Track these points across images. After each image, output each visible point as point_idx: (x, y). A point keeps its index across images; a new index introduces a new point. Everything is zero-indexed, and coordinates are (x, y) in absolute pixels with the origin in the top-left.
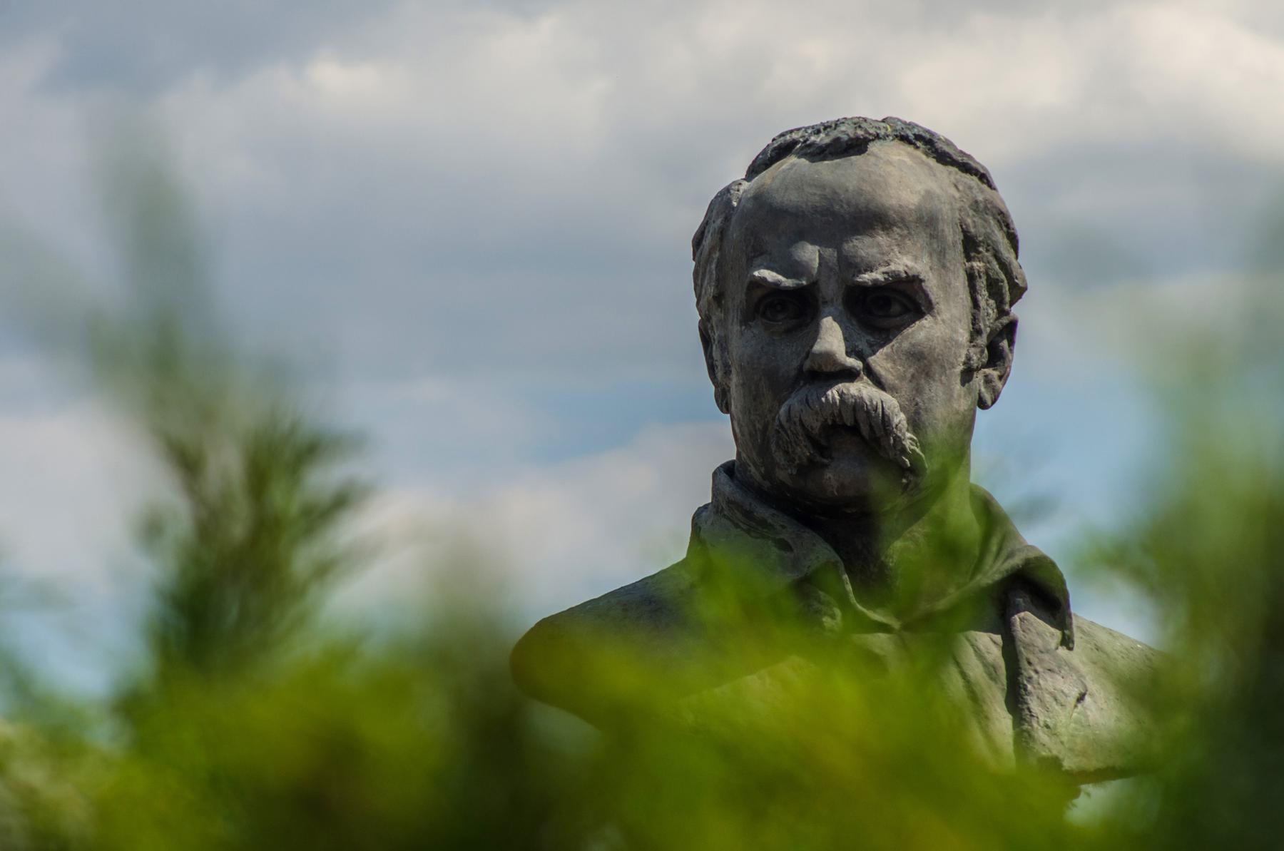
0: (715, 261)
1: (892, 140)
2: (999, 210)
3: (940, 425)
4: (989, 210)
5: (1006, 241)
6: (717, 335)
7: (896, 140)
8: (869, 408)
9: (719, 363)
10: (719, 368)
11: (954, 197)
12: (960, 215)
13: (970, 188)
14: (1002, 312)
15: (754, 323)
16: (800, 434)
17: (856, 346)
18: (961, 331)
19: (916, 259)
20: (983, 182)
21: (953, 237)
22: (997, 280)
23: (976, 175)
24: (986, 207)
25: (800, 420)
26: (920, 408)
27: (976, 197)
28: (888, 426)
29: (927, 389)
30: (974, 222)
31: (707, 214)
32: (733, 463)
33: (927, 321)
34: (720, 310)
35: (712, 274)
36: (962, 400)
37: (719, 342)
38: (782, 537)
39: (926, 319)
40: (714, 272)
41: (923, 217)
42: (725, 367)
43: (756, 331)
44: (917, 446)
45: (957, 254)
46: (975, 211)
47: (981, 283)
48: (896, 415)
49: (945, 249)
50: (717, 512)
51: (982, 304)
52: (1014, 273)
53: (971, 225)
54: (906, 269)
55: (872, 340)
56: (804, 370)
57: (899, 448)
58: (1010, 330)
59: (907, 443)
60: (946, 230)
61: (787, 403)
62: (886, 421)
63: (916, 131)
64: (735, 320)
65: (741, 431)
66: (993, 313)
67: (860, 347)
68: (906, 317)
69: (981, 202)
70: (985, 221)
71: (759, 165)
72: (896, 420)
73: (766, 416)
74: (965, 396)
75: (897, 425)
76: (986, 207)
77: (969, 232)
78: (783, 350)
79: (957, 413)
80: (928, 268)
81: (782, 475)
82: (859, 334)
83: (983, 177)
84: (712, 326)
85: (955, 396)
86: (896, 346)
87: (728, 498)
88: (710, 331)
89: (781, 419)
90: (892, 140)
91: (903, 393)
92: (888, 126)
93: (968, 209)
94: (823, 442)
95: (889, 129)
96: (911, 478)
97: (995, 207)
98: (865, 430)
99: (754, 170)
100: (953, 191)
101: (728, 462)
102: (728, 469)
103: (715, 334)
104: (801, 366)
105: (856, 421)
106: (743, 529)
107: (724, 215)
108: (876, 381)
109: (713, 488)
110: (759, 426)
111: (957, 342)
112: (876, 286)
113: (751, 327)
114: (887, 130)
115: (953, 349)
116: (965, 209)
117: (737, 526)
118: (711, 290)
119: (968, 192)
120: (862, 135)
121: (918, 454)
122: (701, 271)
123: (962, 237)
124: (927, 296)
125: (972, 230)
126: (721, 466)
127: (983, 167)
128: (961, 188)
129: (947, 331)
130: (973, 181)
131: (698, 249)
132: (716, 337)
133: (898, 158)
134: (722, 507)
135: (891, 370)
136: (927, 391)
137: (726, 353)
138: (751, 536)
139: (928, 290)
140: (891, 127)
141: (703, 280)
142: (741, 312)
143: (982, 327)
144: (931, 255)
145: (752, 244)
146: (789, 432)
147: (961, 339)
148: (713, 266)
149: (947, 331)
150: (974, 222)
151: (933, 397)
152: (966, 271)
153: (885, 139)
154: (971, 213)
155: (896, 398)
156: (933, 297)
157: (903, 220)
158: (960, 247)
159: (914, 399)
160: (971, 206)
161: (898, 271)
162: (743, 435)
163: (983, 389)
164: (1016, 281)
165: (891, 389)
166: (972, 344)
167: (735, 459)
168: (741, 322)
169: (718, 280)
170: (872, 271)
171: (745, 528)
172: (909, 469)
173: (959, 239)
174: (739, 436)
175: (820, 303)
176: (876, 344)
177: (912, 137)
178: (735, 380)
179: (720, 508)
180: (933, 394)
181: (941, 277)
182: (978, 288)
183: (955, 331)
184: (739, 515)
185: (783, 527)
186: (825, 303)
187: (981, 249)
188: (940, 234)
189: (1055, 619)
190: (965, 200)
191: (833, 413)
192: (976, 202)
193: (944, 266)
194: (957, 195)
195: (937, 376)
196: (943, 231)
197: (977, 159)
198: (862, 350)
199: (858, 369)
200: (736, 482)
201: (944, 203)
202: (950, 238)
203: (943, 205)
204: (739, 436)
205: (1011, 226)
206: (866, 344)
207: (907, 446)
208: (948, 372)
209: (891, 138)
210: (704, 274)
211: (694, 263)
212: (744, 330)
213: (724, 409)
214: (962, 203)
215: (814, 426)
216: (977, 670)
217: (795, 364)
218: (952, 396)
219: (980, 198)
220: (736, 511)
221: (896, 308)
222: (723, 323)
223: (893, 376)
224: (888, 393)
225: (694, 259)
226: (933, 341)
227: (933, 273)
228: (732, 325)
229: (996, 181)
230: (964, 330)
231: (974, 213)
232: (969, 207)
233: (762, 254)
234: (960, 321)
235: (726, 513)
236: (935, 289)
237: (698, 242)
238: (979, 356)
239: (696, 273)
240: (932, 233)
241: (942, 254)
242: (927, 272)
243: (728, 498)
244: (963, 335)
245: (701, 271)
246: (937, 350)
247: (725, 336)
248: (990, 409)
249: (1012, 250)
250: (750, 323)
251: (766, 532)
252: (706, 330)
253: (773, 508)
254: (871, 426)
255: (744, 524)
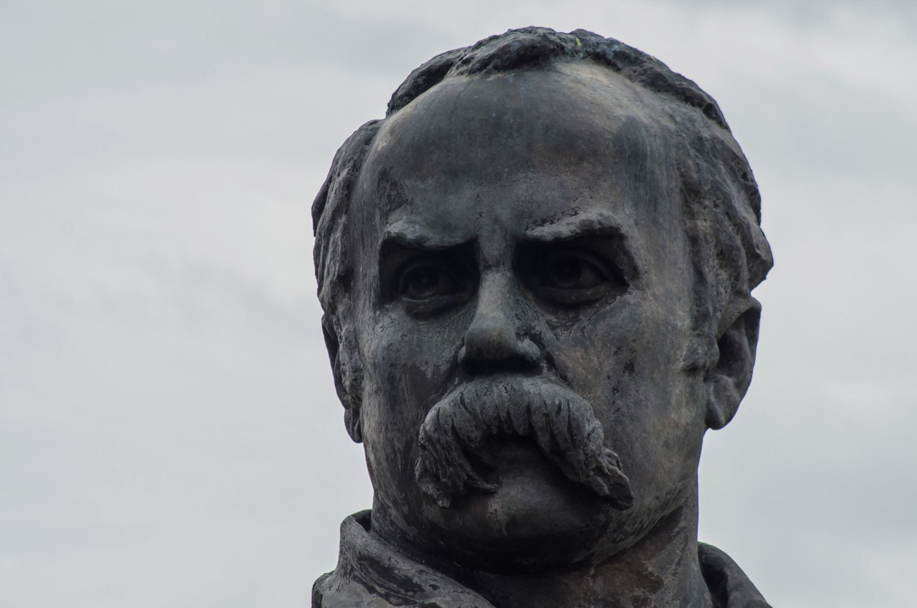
0: (341, 227)
1: (583, 58)
2: (734, 153)
3: (651, 441)
4: (718, 151)
5: (743, 195)
6: (344, 330)
7: (589, 58)
8: (550, 408)
9: (347, 368)
10: (347, 373)
11: (668, 129)
12: (677, 154)
13: (692, 120)
14: (741, 294)
15: (391, 306)
16: (453, 447)
17: (532, 328)
18: (680, 313)
19: (614, 208)
20: (710, 117)
21: (668, 182)
22: (731, 246)
23: (700, 106)
24: (713, 148)
25: (453, 428)
26: (623, 415)
27: (699, 132)
28: (576, 435)
29: (633, 389)
30: (697, 164)
31: (332, 167)
32: (369, 512)
33: (632, 297)
34: (347, 295)
35: (336, 246)
36: (684, 410)
37: (346, 339)
38: (432, 601)
39: (630, 293)
40: (339, 243)
41: (625, 151)
42: (355, 372)
43: (394, 316)
44: (618, 466)
45: (672, 205)
46: (698, 150)
47: (709, 252)
48: (588, 420)
49: (656, 199)
50: (345, 574)
51: (710, 278)
52: (755, 241)
53: (693, 168)
54: (600, 218)
55: (555, 320)
56: (459, 360)
57: (594, 466)
58: (752, 317)
59: (605, 462)
60: (657, 171)
61: (436, 406)
62: (574, 427)
63: (616, 47)
64: (368, 303)
65: (375, 458)
66: (725, 296)
67: (538, 328)
68: (603, 288)
69: (707, 140)
70: (714, 165)
71: (401, 97)
72: (588, 428)
73: (408, 430)
74: (687, 403)
75: (589, 435)
76: (713, 148)
77: (691, 178)
78: (432, 337)
79: (677, 426)
80: (631, 222)
81: (431, 513)
82: (536, 312)
83: (710, 109)
84: (338, 319)
85: (673, 402)
86: (588, 328)
87: (360, 553)
88: (335, 327)
89: (427, 428)
90: (583, 58)
91: (599, 393)
92: (578, 40)
93: (689, 147)
94: (486, 458)
95: (579, 44)
96: (614, 513)
97: (728, 149)
98: (543, 440)
99: (395, 104)
100: (666, 122)
101: (363, 511)
102: (363, 519)
103: (341, 330)
104: (456, 356)
105: (531, 427)
106: (381, 595)
107: (351, 163)
108: (561, 375)
109: (341, 542)
110: (399, 445)
111: (675, 327)
112: (558, 243)
113: (387, 310)
114: (576, 44)
115: (670, 336)
116: (684, 147)
117: (371, 590)
118: (334, 268)
119: (689, 125)
120: (539, 42)
121: (620, 477)
122: (323, 245)
123: (680, 184)
124: (631, 259)
125: (695, 176)
126: (353, 515)
127: (709, 96)
128: (678, 119)
129: (660, 310)
130: (697, 114)
131: (319, 219)
132: (342, 334)
133: (591, 76)
134: (352, 567)
135: (581, 360)
136: (633, 392)
137: (357, 353)
138: (391, 603)
139: (633, 251)
140: (581, 40)
141: (325, 256)
142: (375, 291)
143: (711, 309)
144: (636, 205)
145: (386, 194)
146: (438, 446)
147: (680, 324)
148: (338, 234)
149: (660, 310)
150: (697, 164)
151: (641, 400)
152: (687, 233)
153: (573, 56)
154: (693, 152)
155: (589, 399)
156: (640, 264)
157: (595, 153)
158: (677, 198)
159: (614, 402)
160: (693, 144)
161: (590, 220)
162: (379, 463)
163: (713, 399)
164: (758, 251)
165: (583, 388)
166: (696, 332)
167: (370, 506)
168: (374, 306)
169: (344, 253)
170: (552, 223)
171: (383, 592)
172: (609, 500)
173: (676, 186)
174: (374, 465)
175: (481, 268)
176: (561, 326)
177: (610, 56)
178: (368, 386)
179: (349, 568)
180: (641, 397)
181: (650, 236)
182: (703, 255)
183: (673, 312)
184: (375, 575)
185: (435, 587)
186: (488, 267)
187: (707, 203)
188: (648, 177)
189: (693, 247)
190: (684, 135)
191: (499, 417)
192: (700, 139)
193: (655, 222)
194: (672, 127)
195: (647, 371)
196: (653, 173)
197: (702, 86)
198: (541, 332)
199: (535, 358)
200: (372, 533)
201: (655, 136)
202: (664, 183)
203: (653, 138)
204: (374, 465)
205: (749, 176)
206: (547, 326)
207: (604, 465)
208: (662, 368)
209: (582, 55)
210: (326, 248)
211: (314, 239)
212: (379, 316)
213: (356, 436)
214: (680, 138)
215: (473, 436)
216: (524, 186)
217: (448, 354)
218: (669, 402)
219: (706, 134)
220: (370, 570)
221: (587, 276)
222: (351, 312)
223: (584, 369)
224: (578, 392)
225: (315, 235)
226: (641, 323)
227: (639, 230)
228: (363, 312)
229: (729, 118)
230: (684, 312)
231: (697, 154)
232: (690, 144)
233: (399, 206)
234: (679, 299)
235: (357, 573)
236: (642, 252)
237: (318, 208)
238: (706, 349)
239: (317, 248)
240: (637, 173)
241: (654, 203)
242: (630, 227)
243: (360, 553)
244: (683, 319)
245: (323, 245)
246: (646, 335)
247: (355, 329)
248: (723, 429)
249: (752, 210)
250: (387, 306)
251: (412, 597)
252: (331, 327)
253: (422, 564)
254: (552, 434)
255: (381, 586)
